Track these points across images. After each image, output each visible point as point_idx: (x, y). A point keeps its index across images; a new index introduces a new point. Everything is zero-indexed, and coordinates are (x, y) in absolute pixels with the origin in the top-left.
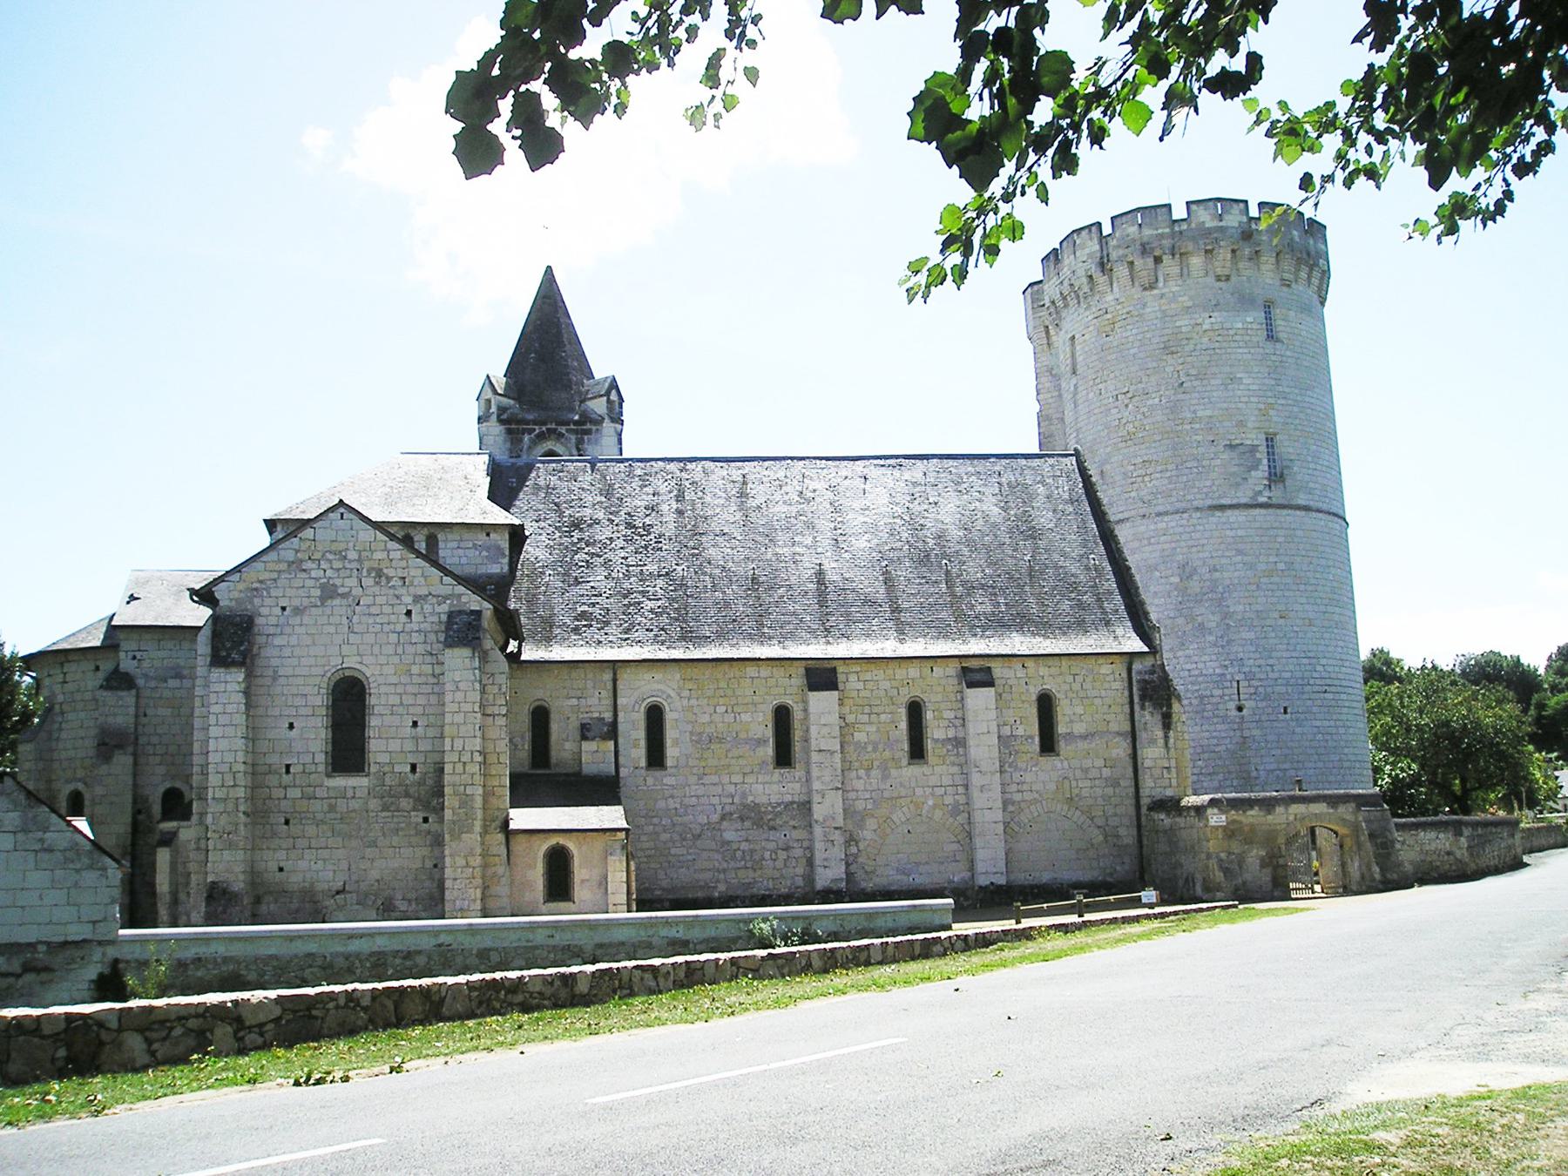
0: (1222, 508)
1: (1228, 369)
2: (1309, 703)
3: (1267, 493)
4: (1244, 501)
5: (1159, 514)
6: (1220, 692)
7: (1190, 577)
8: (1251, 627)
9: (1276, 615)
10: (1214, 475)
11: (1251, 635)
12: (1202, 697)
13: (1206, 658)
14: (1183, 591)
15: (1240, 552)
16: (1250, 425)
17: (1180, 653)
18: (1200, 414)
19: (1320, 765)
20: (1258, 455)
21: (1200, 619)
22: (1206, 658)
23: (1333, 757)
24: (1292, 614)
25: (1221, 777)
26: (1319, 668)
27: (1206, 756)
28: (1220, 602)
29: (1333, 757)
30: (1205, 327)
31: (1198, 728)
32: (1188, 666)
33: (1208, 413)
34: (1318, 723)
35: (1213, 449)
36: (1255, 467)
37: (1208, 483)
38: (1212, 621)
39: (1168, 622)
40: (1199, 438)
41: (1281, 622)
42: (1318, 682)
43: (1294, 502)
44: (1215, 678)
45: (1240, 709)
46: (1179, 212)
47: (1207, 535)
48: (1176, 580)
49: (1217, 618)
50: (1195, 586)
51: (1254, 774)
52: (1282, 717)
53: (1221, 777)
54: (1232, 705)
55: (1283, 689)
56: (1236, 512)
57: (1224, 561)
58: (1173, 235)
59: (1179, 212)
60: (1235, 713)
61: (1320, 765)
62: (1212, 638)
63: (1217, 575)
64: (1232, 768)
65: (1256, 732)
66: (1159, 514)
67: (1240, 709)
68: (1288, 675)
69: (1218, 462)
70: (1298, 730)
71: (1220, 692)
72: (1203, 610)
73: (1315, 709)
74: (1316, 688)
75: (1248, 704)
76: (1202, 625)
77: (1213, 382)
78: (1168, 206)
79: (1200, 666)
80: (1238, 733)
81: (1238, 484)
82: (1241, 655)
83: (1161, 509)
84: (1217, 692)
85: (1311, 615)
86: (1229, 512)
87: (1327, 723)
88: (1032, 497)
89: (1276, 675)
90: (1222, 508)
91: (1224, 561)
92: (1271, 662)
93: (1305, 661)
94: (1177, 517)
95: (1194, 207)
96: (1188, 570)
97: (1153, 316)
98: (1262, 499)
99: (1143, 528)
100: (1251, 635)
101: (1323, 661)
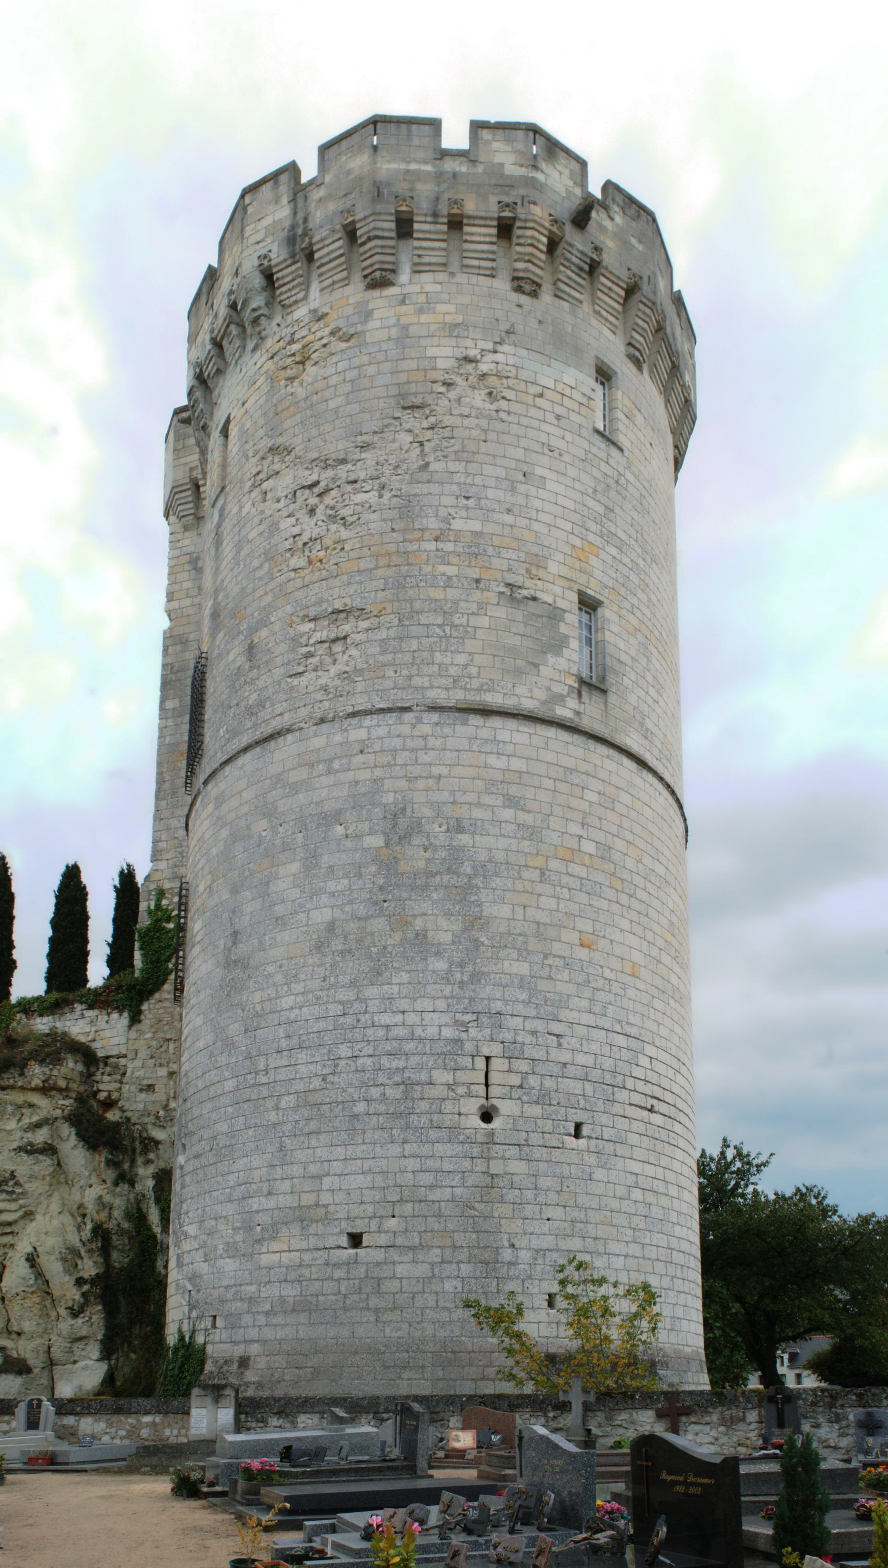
0: (486, 712)
1: (519, 454)
2: (621, 1123)
3: (572, 703)
4: (529, 705)
5: (353, 715)
6: (448, 1077)
7: (405, 838)
8: (523, 953)
9: (574, 937)
10: (471, 645)
11: (522, 968)
12: (408, 1084)
13: (427, 1004)
14: (389, 865)
15: (512, 802)
16: (553, 567)
17: (371, 992)
18: (457, 524)
19: (634, 1250)
20: (563, 629)
21: (419, 923)
22: (427, 1004)
23: (657, 1239)
24: (602, 944)
25: (435, 1255)
26: (644, 1061)
27: (408, 1208)
28: (464, 894)
29: (657, 1239)
30: (484, 367)
31: (396, 1150)
32: (386, 1019)
33: (476, 526)
34: (636, 1167)
35: (477, 595)
36: (557, 645)
37: (461, 659)
38: (445, 931)
39: (354, 926)
40: (451, 570)
41: (582, 953)
42: (640, 1086)
43: (621, 739)
44: (439, 1047)
45: (487, 1116)
46: (455, 137)
47: (450, 756)
48: (377, 841)
49: (456, 926)
50: (415, 858)
51: (507, 1254)
52: (571, 1142)
53: (435, 1255)
54: (473, 1106)
55: (576, 1087)
56: (511, 724)
57: (477, 813)
58: (439, 176)
59: (455, 137)
60: (476, 1121)
61: (634, 1250)
62: (440, 965)
63: (464, 839)
64: (460, 1239)
65: (518, 1167)
66: (353, 715)
67: (487, 1116)
68: (589, 1060)
69: (485, 622)
70: (600, 1174)
71: (448, 1077)
72: (426, 906)
73: (633, 1139)
74: (636, 1099)
75: (506, 1107)
76: (421, 936)
77: (488, 470)
78: (434, 125)
79: (412, 1018)
80: (480, 1166)
81: (518, 672)
82: (498, 1006)
83: (361, 702)
84: (443, 1077)
85: (637, 957)
86: (496, 722)
87: (650, 1170)
88: (480, 1536)
89: (566, 1057)
90: (486, 712)
91: (477, 813)
92: (556, 1028)
93: (621, 1041)
94: (391, 718)
95: (486, 135)
96: (402, 822)
97: (382, 335)
98: (564, 712)
99: (318, 742)
100: (522, 968)
101: (650, 1050)
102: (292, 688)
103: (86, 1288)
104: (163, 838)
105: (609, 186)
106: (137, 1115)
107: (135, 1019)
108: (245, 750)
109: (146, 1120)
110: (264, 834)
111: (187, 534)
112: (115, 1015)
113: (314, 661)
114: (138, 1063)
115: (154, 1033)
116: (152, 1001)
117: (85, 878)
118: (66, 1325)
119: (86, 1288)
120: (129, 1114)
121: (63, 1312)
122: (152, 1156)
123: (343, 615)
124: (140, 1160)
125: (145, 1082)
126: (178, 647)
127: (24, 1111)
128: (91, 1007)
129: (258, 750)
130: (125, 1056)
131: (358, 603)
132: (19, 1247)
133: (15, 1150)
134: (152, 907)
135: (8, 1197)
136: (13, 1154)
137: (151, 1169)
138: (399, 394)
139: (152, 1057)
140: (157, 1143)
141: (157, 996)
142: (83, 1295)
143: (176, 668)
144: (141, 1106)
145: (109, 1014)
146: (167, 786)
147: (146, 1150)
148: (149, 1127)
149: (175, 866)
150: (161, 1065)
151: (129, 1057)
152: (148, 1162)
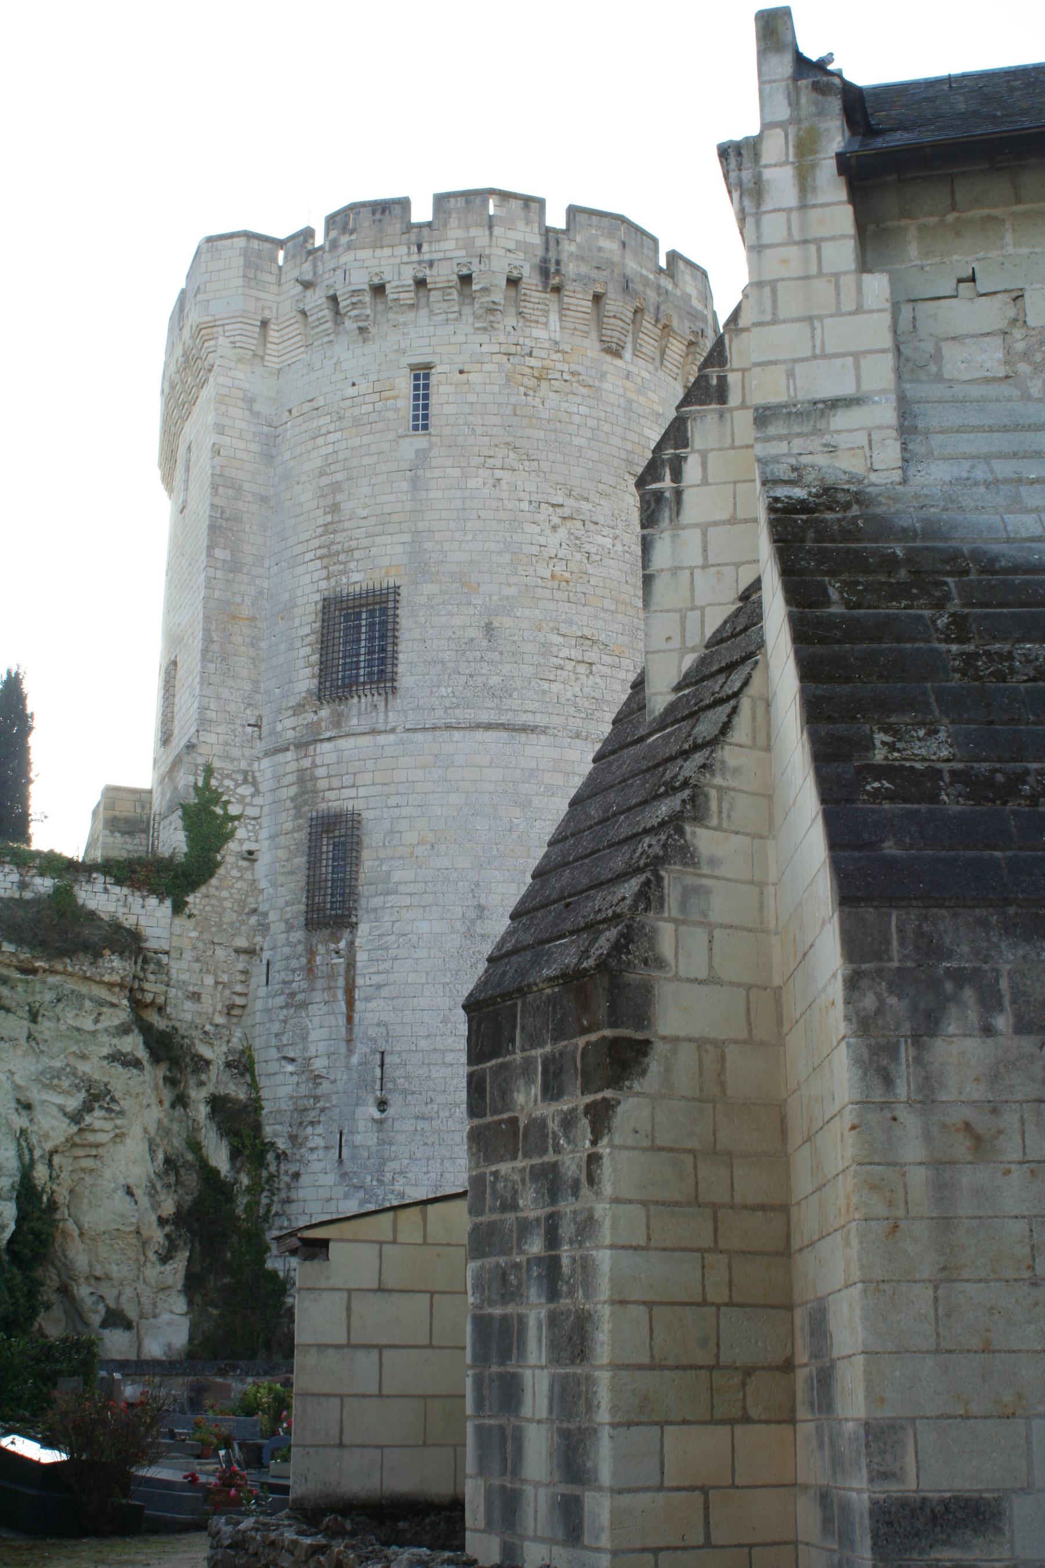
102: (544, 692)
103: (167, 1229)
104: (212, 707)
105: (574, 212)
106: (185, 1026)
107: (178, 908)
108: (489, 727)
109: (194, 1033)
110: (516, 821)
111: (240, 366)
112: (153, 901)
113: (563, 674)
114: (183, 965)
115: (201, 933)
116: (198, 895)
117: (27, 687)
118: (153, 1272)
119: (167, 1229)
120: (177, 1024)
121: (152, 1257)
122: (203, 1077)
123: (589, 643)
124: (192, 1082)
125: (191, 988)
126: (230, 492)
127: (105, 1010)
128: (119, 882)
129: (504, 734)
130: (167, 953)
131: (603, 637)
132: (107, 1173)
133: (105, 1058)
134: (200, 784)
135: (107, 1115)
136: (105, 1063)
137: (203, 1093)
138: (627, 460)
139: (197, 960)
140: (208, 1063)
141: (203, 889)
142: (168, 1236)
143: (227, 515)
144: (188, 1017)
145: (143, 898)
146: (215, 647)
147: (197, 1071)
148: (197, 1041)
149: (227, 744)
150: (208, 972)
151: (173, 954)
152: (201, 1084)
